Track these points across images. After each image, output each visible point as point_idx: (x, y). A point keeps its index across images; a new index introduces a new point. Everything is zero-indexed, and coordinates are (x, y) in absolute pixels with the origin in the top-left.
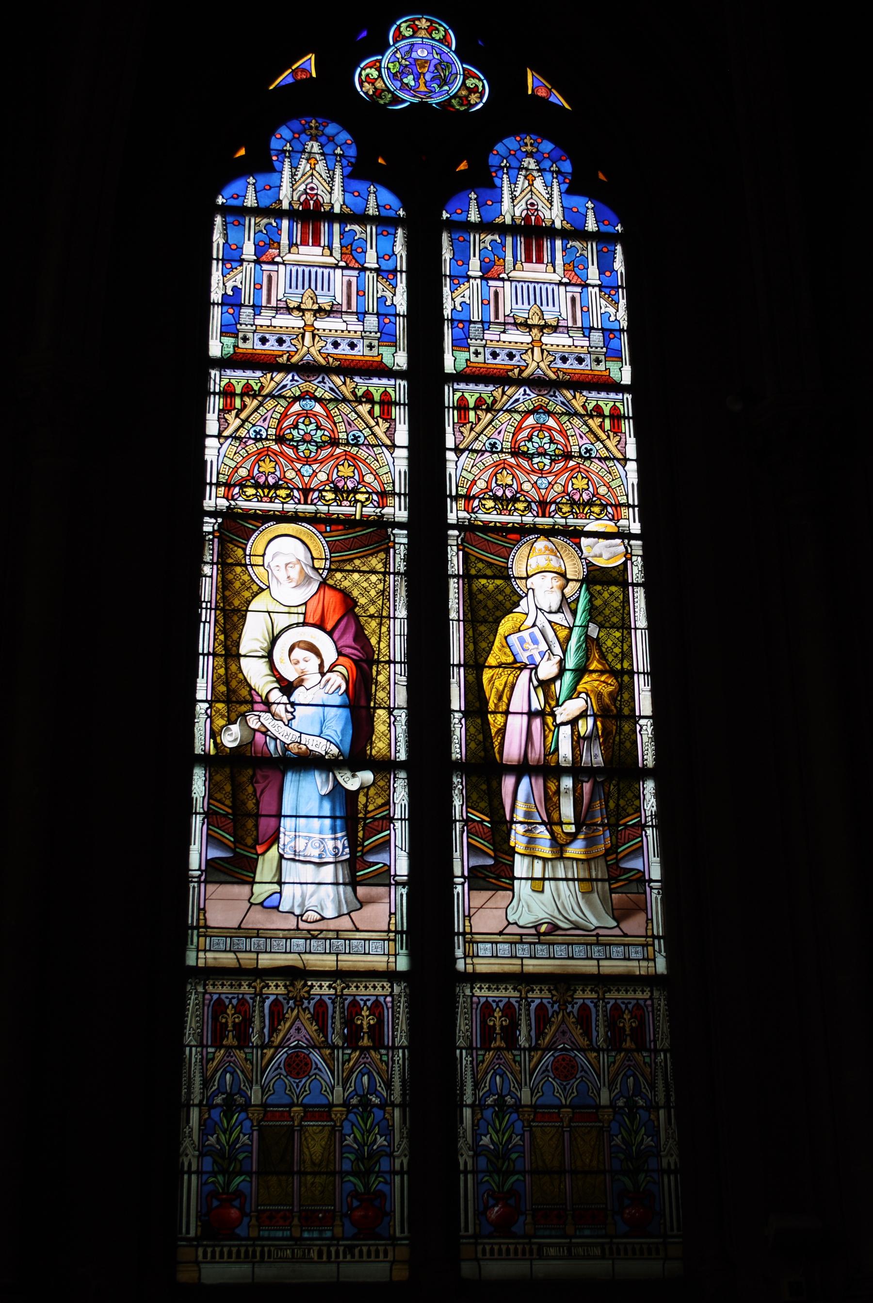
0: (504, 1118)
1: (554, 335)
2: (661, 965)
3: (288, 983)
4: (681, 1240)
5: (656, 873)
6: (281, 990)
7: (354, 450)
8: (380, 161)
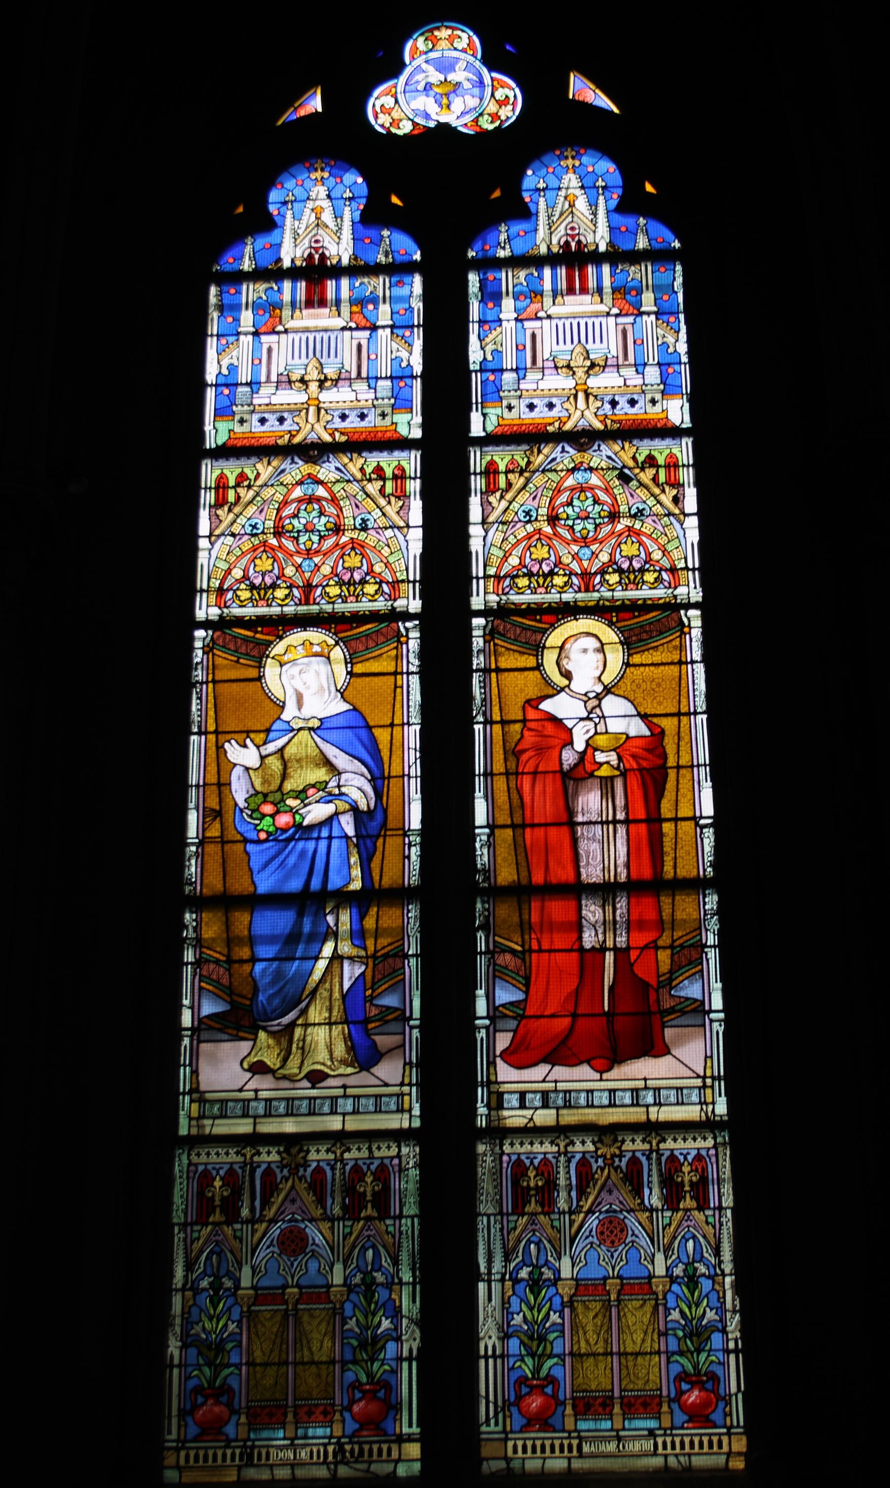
1: (603, 375)
2: (721, 1108)
3: (282, 1149)
4: (167, 1444)
5: (717, 1002)
6: (274, 1157)
7: (363, 536)
8: (395, 200)
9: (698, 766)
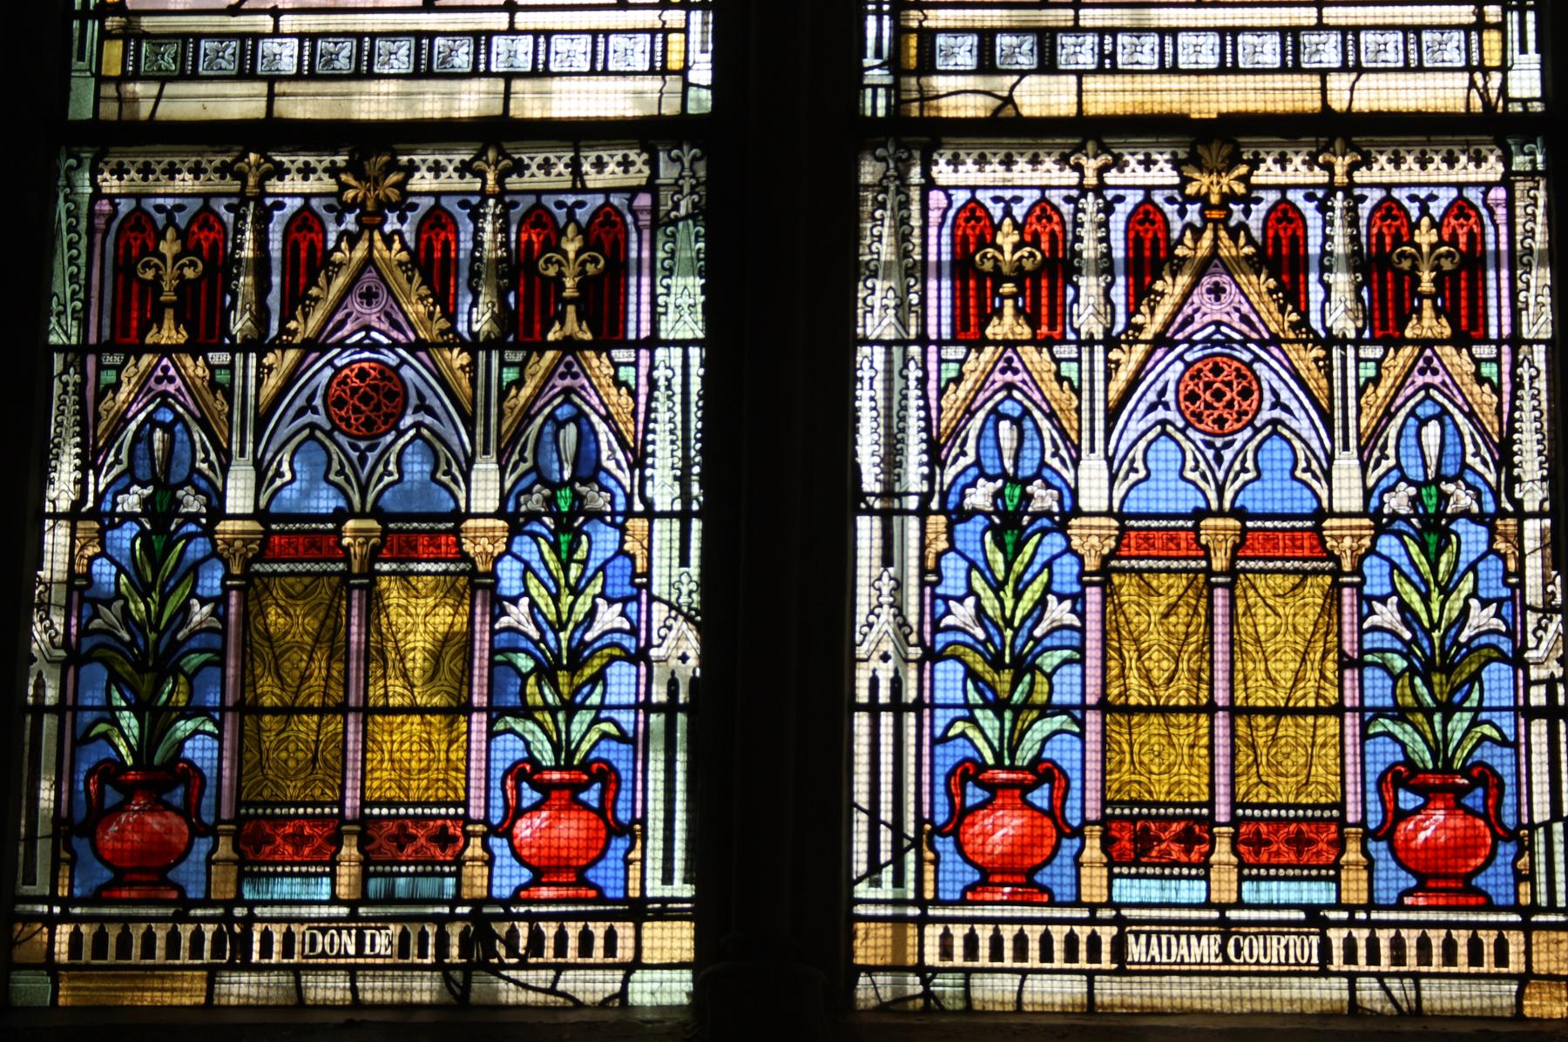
0: (1019, 549)
2: (1526, 81)
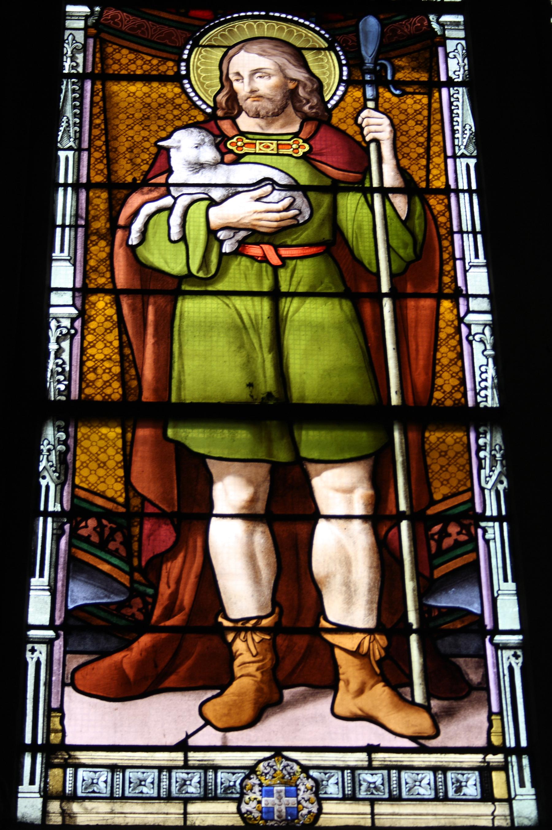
5: (509, 615)
9: (457, 191)
